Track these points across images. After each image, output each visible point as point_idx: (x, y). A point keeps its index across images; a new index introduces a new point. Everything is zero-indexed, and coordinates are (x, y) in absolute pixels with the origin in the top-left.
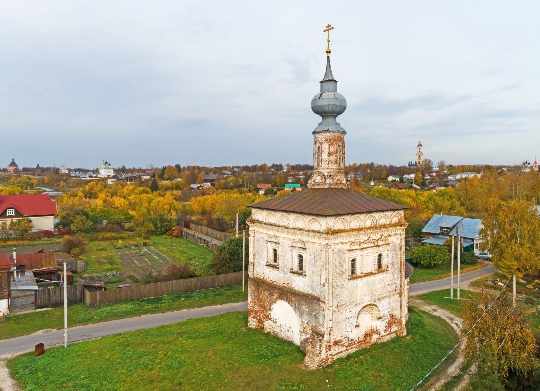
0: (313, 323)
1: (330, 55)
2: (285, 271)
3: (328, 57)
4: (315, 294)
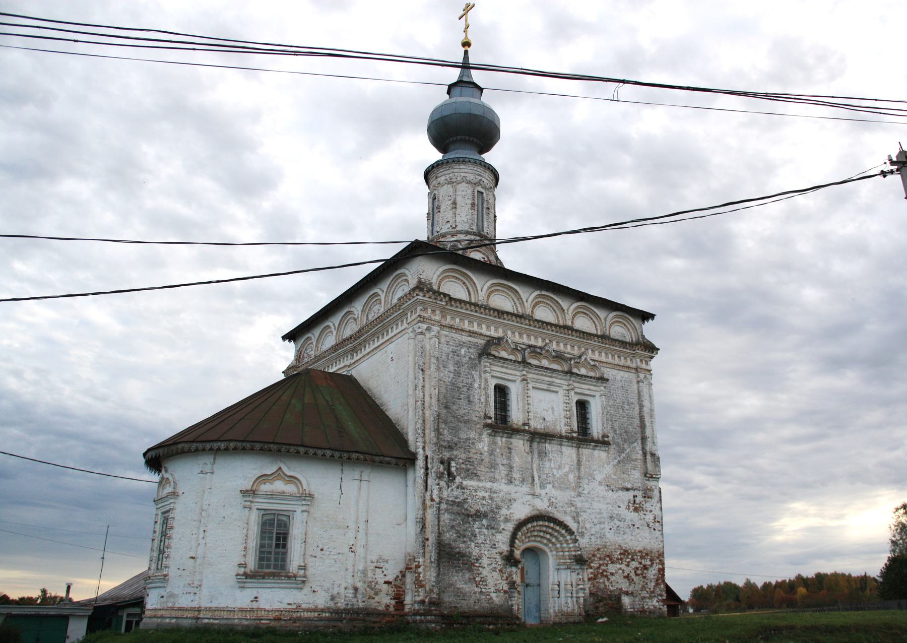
3: (466, 52)
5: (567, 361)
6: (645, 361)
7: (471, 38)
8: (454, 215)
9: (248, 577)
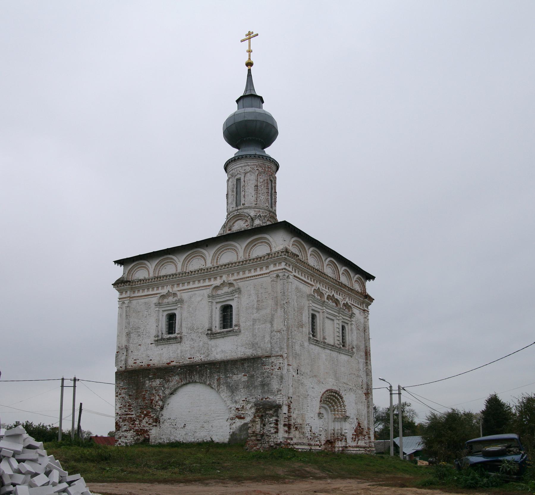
0: (258, 395)
3: (249, 70)
4: (260, 353)
5: (510, 451)
6: (304, 275)
7: (252, 60)
8: (256, 191)
9: (159, 341)
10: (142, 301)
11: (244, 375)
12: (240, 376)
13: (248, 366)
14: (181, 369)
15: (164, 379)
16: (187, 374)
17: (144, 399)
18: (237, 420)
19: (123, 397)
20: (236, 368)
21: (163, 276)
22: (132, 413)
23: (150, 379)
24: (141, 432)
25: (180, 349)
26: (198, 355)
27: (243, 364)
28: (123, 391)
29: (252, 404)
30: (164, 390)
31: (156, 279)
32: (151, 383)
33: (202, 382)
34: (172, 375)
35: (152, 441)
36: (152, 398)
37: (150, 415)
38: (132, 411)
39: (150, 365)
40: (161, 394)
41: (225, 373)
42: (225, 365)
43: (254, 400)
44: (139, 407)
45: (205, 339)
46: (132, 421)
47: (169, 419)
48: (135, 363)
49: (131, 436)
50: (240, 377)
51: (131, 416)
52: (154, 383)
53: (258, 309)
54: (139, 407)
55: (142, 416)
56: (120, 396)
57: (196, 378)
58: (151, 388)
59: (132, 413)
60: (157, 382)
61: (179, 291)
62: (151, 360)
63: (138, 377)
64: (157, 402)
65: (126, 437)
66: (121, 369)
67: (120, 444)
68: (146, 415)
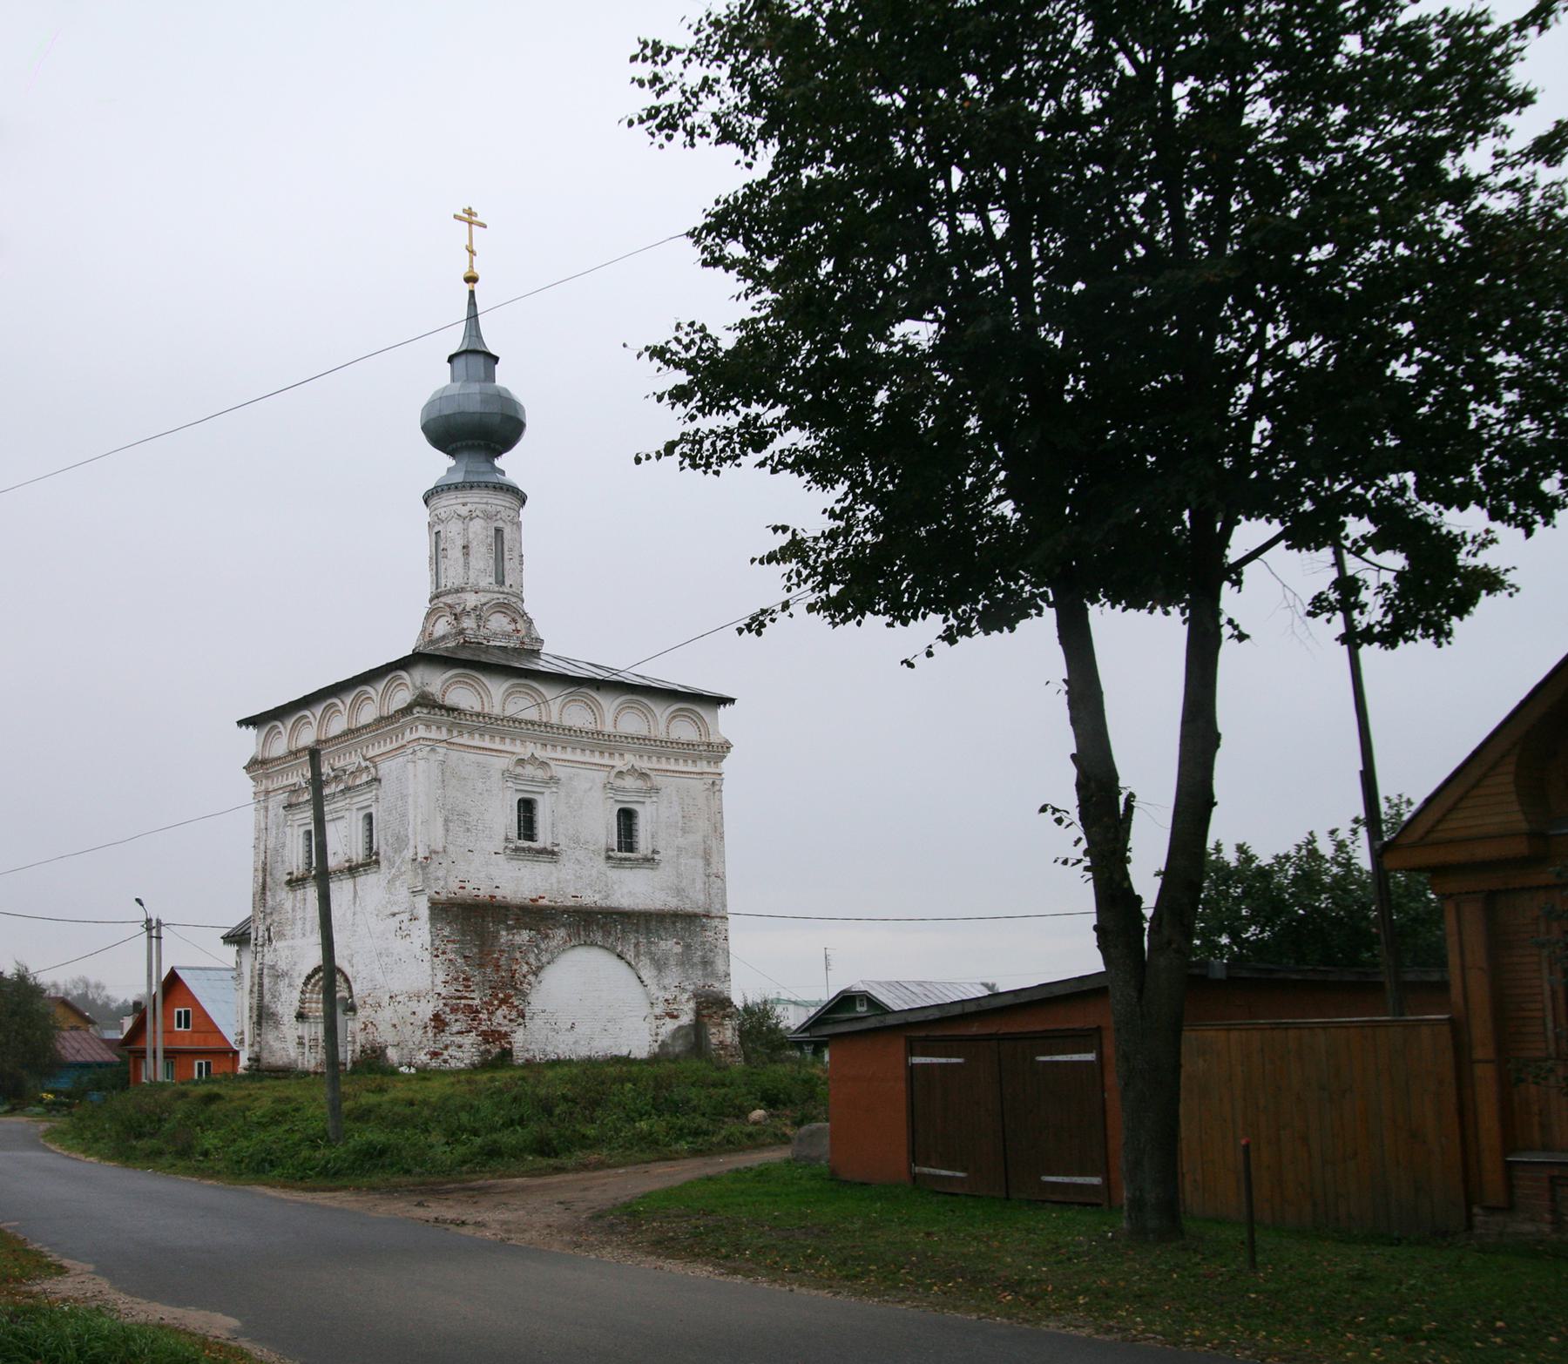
0: (697, 979)
1: (477, 287)
2: (581, 858)
3: (472, 293)
4: (688, 907)
7: (477, 270)
10: (471, 757)
11: (677, 943)
12: (671, 943)
13: (682, 929)
14: (569, 916)
15: (539, 932)
16: (581, 928)
17: (497, 967)
18: (668, 1019)
19: (450, 960)
20: (665, 928)
21: (527, 722)
22: (473, 995)
23: (509, 929)
24: (491, 1036)
25: (555, 875)
26: (589, 892)
27: (674, 923)
28: (450, 946)
29: (689, 994)
30: (539, 954)
31: (595, 736)
32: (511, 937)
33: (608, 946)
34: (554, 925)
35: (520, 1056)
36: (514, 967)
37: (512, 1003)
38: (473, 991)
39: (495, 897)
40: (532, 960)
41: (647, 934)
42: (647, 921)
43: (692, 987)
44: (487, 984)
45: (601, 863)
46: (473, 1012)
47: (543, 1011)
48: (461, 888)
49: (472, 1044)
50: (669, 946)
51: (470, 1002)
52: (517, 938)
53: (684, 831)
54: (487, 984)
55: (496, 1002)
56: (442, 957)
57: (598, 937)
58: (512, 945)
59: (473, 995)
60: (524, 936)
61: (553, 759)
62: (497, 887)
63: (483, 921)
64: (525, 976)
65: (460, 1047)
66: (437, 896)
67: (445, 1061)
68: (503, 1002)
